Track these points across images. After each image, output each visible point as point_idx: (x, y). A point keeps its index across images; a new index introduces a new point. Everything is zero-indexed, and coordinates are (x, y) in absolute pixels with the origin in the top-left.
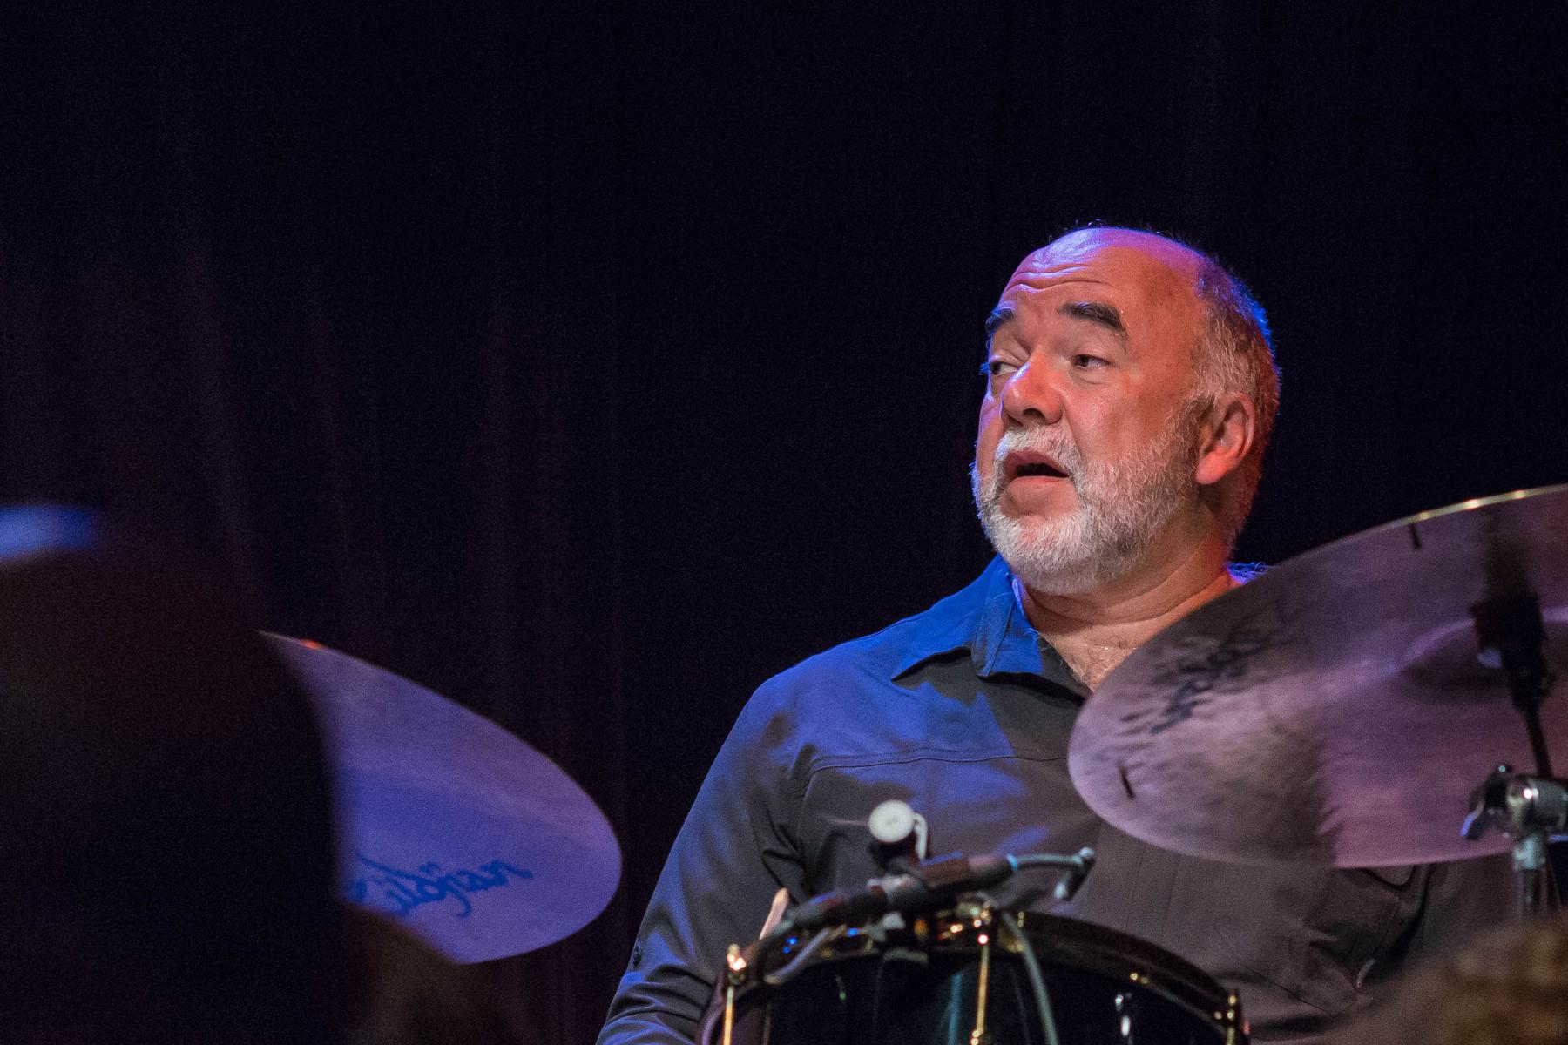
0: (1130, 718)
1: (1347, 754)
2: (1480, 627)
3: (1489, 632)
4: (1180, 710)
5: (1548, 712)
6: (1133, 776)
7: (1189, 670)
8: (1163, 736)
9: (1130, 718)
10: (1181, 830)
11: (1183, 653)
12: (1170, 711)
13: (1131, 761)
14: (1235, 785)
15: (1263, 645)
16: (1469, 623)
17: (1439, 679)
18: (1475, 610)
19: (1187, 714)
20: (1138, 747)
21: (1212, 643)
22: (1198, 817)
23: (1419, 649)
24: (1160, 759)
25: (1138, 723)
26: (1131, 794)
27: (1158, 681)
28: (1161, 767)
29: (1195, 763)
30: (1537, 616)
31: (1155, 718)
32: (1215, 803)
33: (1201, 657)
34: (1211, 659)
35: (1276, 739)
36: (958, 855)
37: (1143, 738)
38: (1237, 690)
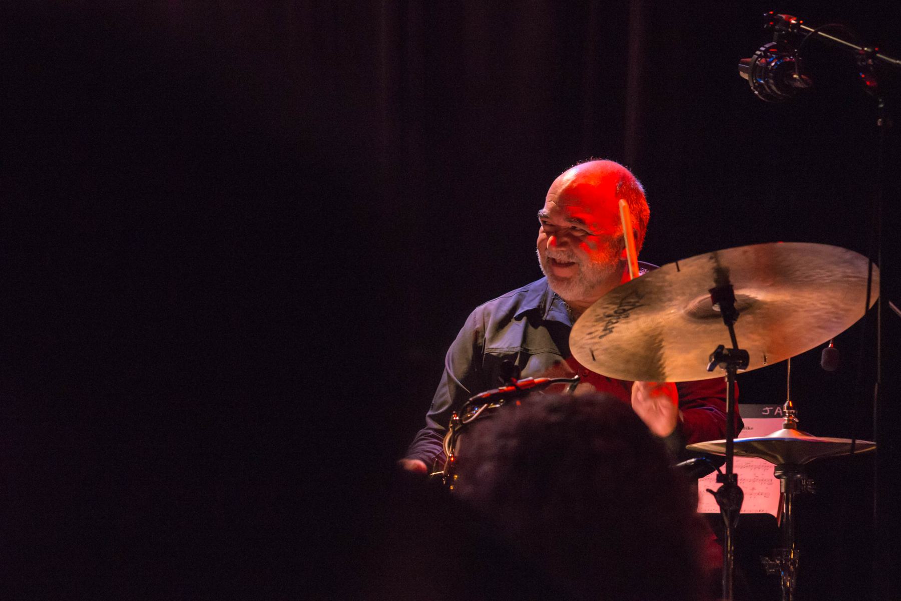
0: (590, 333)
1: (502, 325)
2: (712, 297)
3: (715, 300)
4: (608, 330)
5: (737, 325)
6: (595, 353)
7: (609, 316)
8: (604, 339)
9: (590, 333)
10: (616, 371)
11: (604, 311)
12: (604, 330)
13: (594, 348)
14: (633, 355)
15: (634, 307)
16: (709, 295)
17: (701, 316)
18: (712, 291)
19: (611, 332)
20: (596, 343)
21: (615, 307)
22: (622, 367)
23: (693, 304)
24: (605, 347)
25: (593, 335)
26: (594, 359)
27: (597, 321)
28: (606, 350)
29: (618, 348)
30: (733, 292)
31: (600, 333)
32: (628, 361)
33: (612, 312)
34: (616, 312)
35: (646, 338)
36: (531, 378)
37: (597, 340)
38: (627, 323)
